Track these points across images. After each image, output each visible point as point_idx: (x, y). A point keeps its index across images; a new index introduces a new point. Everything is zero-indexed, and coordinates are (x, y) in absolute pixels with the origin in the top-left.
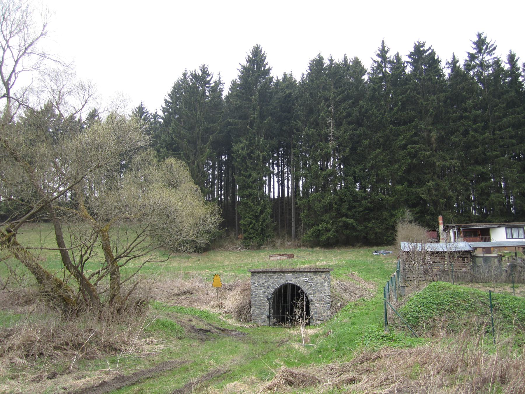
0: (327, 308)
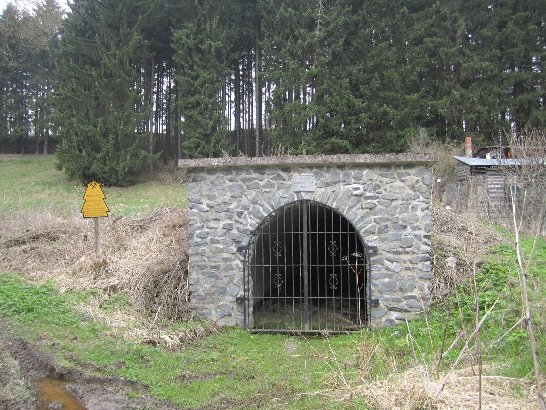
0: (421, 274)
